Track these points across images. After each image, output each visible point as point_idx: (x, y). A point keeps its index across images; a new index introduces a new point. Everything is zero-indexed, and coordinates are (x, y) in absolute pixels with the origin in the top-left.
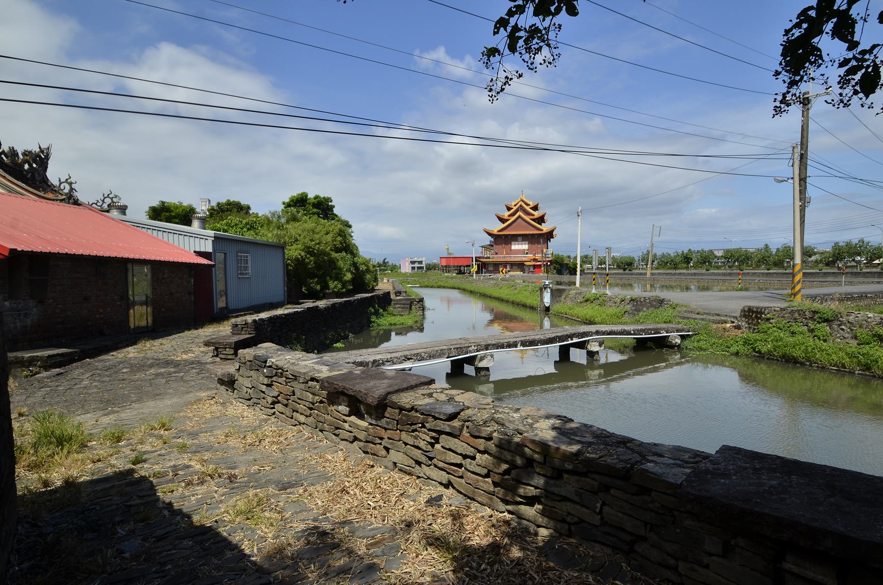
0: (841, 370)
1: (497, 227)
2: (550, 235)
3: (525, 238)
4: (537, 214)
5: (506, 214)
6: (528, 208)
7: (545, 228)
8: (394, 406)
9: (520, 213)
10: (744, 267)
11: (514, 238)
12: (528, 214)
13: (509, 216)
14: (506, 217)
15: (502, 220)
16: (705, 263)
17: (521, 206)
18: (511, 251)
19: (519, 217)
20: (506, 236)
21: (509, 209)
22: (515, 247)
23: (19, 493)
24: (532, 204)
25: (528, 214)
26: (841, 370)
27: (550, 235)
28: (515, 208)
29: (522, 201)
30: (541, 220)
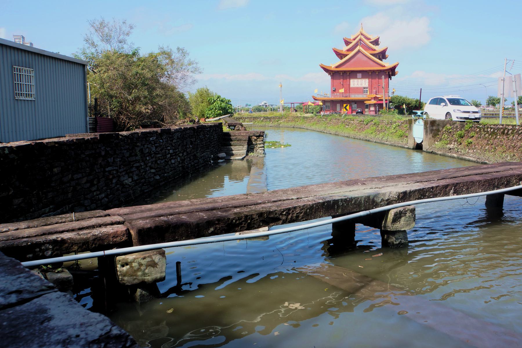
0: (471, 290)
1: (334, 62)
2: (391, 72)
3: (365, 74)
4: (378, 49)
5: (344, 48)
6: (367, 42)
7: (387, 64)
8: (123, 342)
9: (359, 48)
10: (124, 62)
11: (353, 74)
12: (368, 48)
13: (349, 50)
14: (344, 52)
15: (340, 55)
16: (112, 64)
17: (360, 40)
18: (349, 90)
19: (359, 51)
20: (345, 72)
21: (347, 43)
22: (355, 83)
23: (356, 224)
24: (373, 38)
25: (368, 48)
26: (471, 290)
27: (391, 72)
28: (354, 42)
29: (362, 34)
30: (382, 55)
